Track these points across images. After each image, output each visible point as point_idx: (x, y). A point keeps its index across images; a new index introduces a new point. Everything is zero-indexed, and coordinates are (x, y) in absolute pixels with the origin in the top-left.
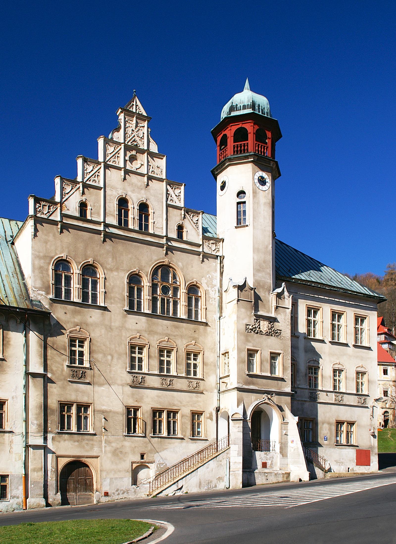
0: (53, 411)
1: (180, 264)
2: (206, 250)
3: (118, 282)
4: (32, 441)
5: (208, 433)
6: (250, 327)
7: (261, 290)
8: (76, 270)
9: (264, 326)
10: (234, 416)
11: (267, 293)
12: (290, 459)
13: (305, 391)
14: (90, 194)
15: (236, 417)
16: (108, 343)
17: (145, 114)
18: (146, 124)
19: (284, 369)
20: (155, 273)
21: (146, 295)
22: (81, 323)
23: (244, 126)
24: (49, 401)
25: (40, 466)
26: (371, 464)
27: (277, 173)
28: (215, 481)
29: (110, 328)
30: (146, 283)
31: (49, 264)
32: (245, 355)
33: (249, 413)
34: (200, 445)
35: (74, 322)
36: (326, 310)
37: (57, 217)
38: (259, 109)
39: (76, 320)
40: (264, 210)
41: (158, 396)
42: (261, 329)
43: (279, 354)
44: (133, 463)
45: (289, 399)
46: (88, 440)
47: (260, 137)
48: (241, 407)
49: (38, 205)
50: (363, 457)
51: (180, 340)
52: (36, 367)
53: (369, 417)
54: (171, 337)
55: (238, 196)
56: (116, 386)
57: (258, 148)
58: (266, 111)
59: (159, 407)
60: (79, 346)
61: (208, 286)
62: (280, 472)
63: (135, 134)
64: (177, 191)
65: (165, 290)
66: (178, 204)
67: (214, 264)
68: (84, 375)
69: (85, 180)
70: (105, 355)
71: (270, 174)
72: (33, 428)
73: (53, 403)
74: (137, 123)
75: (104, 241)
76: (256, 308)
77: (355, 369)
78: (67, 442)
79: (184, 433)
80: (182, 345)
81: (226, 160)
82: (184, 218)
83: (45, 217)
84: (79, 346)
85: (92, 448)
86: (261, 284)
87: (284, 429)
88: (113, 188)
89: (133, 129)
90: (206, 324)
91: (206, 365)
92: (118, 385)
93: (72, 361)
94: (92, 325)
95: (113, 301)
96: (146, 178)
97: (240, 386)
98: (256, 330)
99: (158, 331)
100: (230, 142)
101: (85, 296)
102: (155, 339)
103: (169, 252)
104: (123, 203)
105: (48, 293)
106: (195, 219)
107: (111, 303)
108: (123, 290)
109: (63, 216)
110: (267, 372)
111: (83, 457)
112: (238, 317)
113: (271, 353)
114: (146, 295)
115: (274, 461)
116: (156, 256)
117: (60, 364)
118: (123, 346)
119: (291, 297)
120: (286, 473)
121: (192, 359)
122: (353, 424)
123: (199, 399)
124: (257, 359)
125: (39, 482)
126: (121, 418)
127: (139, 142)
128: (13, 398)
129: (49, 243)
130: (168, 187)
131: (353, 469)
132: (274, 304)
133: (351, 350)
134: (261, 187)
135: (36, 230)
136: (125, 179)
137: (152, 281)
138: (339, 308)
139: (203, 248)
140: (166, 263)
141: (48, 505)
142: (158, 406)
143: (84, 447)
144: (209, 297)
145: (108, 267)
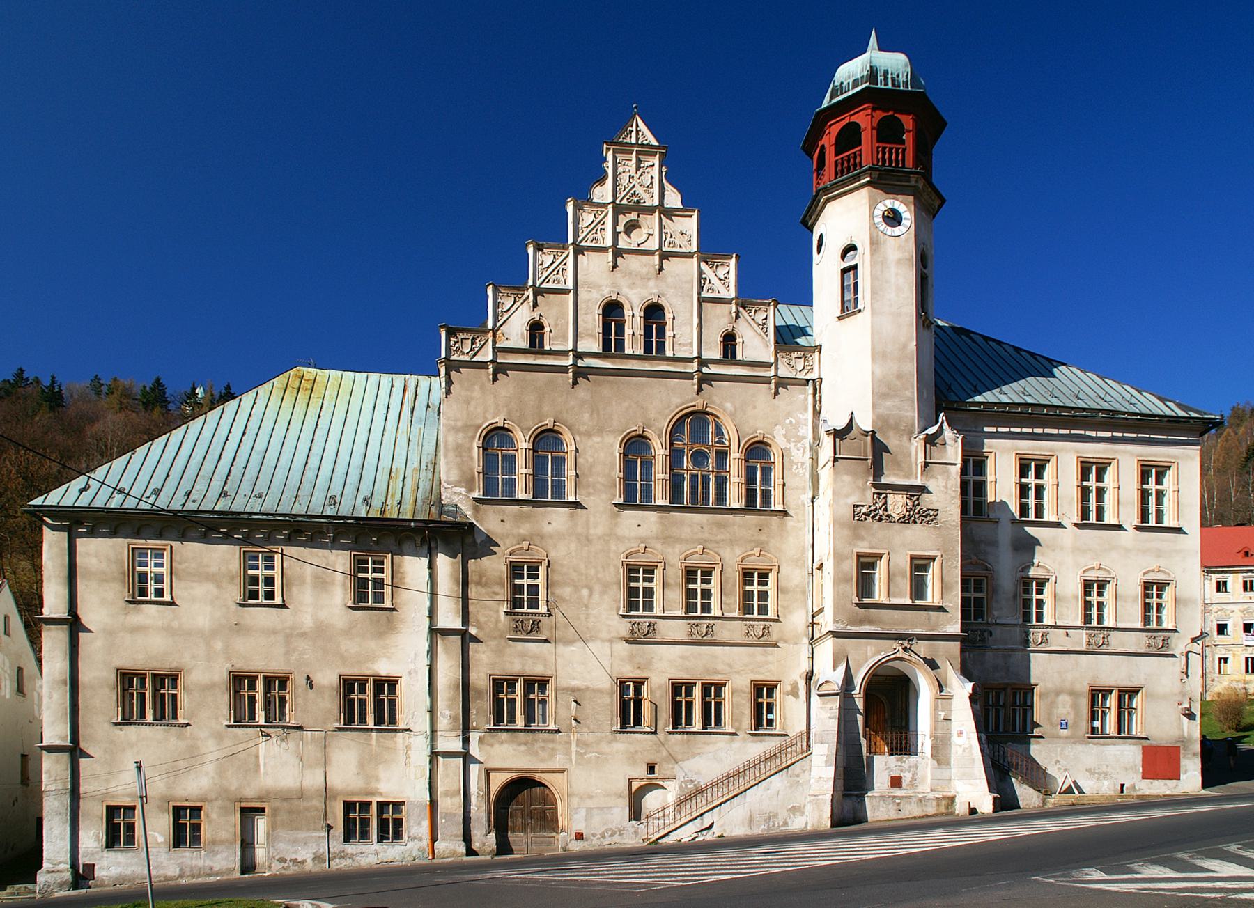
0: (479, 692)
1: (729, 406)
2: (784, 372)
3: (602, 455)
4: (441, 746)
5: (788, 722)
6: (864, 510)
7: (891, 434)
8: (523, 442)
9: (897, 504)
10: (823, 688)
11: (905, 438)
12: (954, 770)
13: (1012, 628)
14: (548, 304)
15: (827, 689)
16: (582, 566)
17: (655, 143)
18: (656, 160)
19: (945, 588)
20: (677, 427)
21: (659, 474)
22: (531, 536)
23: (853, 119)
24: (473, 676)
25: (455, 787)
26: (1182, 777)
27: (934, 196)
28: (783, 814)
29: (587, 540)
30: (659, 450)
31: (473, 437)
32: (851, 567)
33: (859, 679)
34: (769, 745)
35: (519, 535)
36: (1065, 459)
37: (486, 355)
38: (886, 79)
39: (522, 531)
40: (897, 274)
41: (683, 657)
42: (889, 512)
43: (933, 559)
44: (631, 781)
45: (956, 646)
46: (544, 741)
47: (888, 132)
48: (842, 669)
49: (454, 340)
50: (1160, 761)
51: (728, 550)
52: (449, 618)
53: (1178, 675)
54: (709, 546)
55: (843, 258)
56: (599, 643)
57: (884, 154)
58: (902, 79)
59: (685, 676)
60: (760, 583)
61: (789, 441)
62: (931, 795)
63: (635, 182)
64: (722, 271)
65: (699, 458)
66: (724, 294)
67: (802, 397)
68: (536, 626)
69: (538, 283)
70: (577, 588)
71: (911, 198)
72: (443, 723)
73: (479, 678)
74: (639, 162)
75: (575, 383)
76: (878, 470)
77: (1140, 575)
78: (505, 746)
79: (737, 724)
80: (732, 558)
81: (818, 192)
82: (737, 317)
83: (466, 358)
84: (760, 583)
85: (552, 755)
86: (892, 422)
87: (946, 710)
88: (592, 286)
89: (635, 172)
90: (785, 514)
91: (179, 579)
92: (603, 641)
93: (516, 603)
94: (551, 536)
95: (591, 490)
96: (657, 258)
97: (840, 627)
98: (878, 515)
99: (683, 536)
100: (830, 158)
101: (750, 496)
102: (677, 550)
103: (704, 386)
104: (612, 310)
105: (470, 490)
106: (760, 317)
107: (589, 494)
108: (612, 467)
109: (496, 350)
110: (901, 595)
111: (536, 771)
112: (834, 493)
113: (912, 558)
114: (659, 474)
115: (920, 773)
116: (681, 396)
117: (493, 612)
118: (612, 569)
119: (960, 440)
120: (944, 798)
121: (756, 583)
122: (1137, 692)
123: (770, 658)
124: (880, 574)
125: (455, 815)
126: (609, 701)
127: (645, 196)
128: (410, 673)
129: (473, 403)
130: (703, 265)
131: (1133, 787)
132: (921, 459)
133: (1130, 537)
134: (889, 230)
135: (449, 382)
136: (615, 266)
137: (671, 444)
138: (1095, 452)
139: (777, 369)
140: (699, 408)
141: (470, 852)
142: (682, 675)
143: (536, 754)
144: (791, 462)
145: (583, 429)
